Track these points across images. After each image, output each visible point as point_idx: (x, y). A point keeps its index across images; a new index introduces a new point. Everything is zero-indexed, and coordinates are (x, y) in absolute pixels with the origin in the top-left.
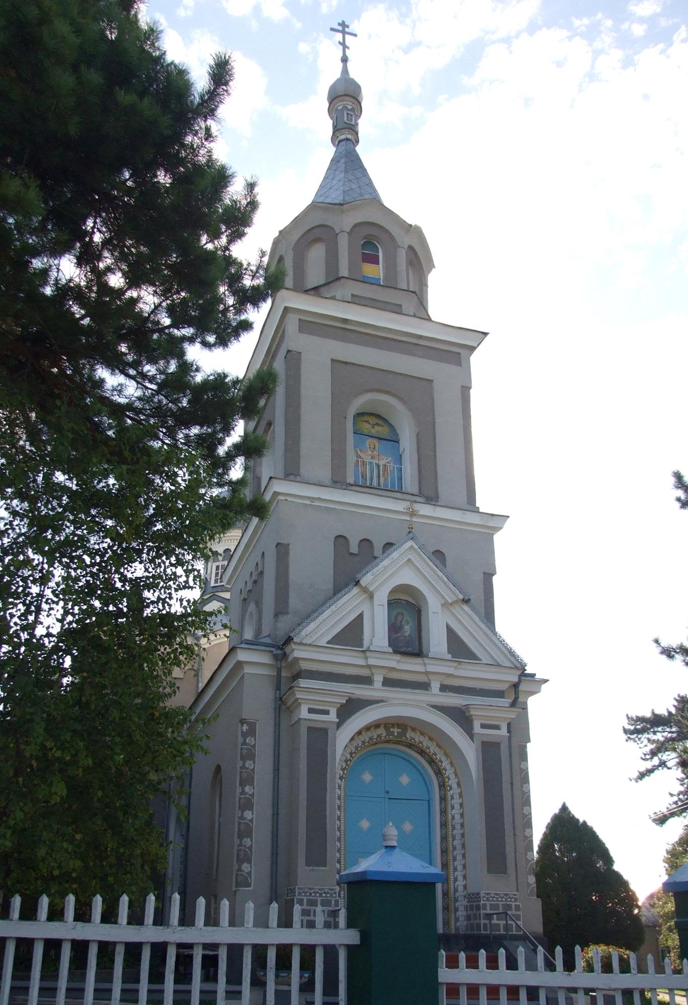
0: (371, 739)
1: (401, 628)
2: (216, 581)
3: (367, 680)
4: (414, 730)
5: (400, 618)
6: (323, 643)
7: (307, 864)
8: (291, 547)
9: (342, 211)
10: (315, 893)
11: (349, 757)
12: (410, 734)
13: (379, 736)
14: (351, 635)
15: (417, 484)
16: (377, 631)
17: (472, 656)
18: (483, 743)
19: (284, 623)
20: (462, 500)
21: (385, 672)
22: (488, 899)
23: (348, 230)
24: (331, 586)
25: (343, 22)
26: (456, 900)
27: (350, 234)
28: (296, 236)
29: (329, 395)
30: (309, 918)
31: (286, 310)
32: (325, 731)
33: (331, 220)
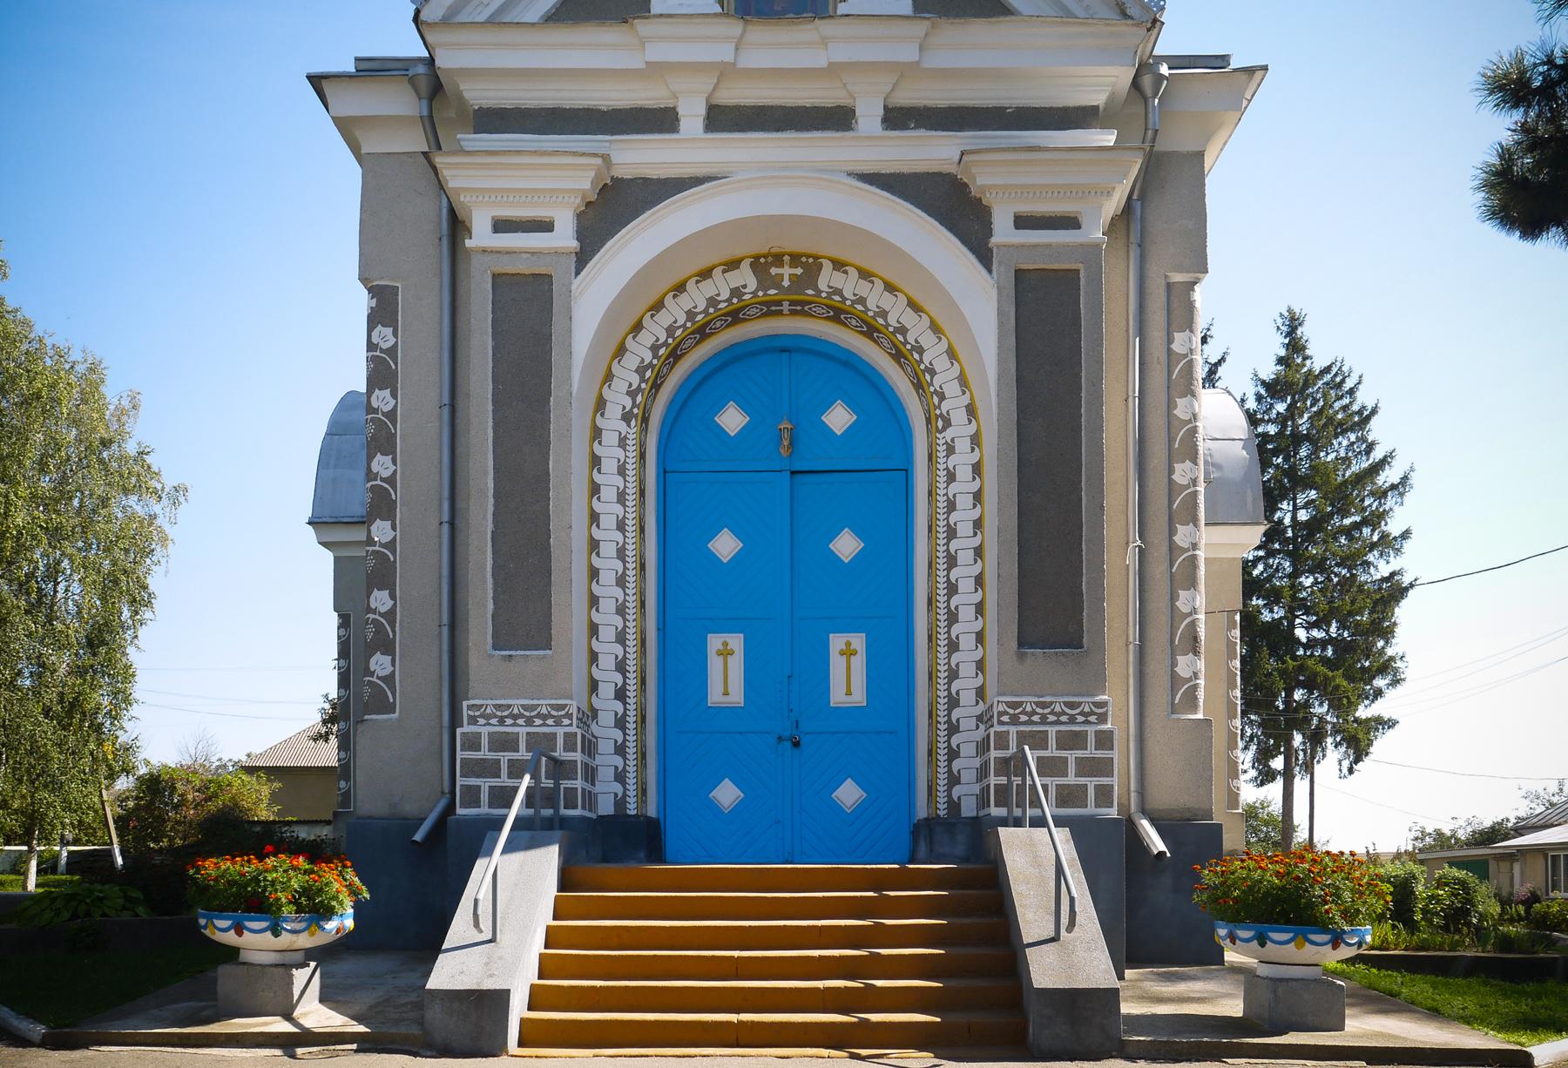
3: (661, 120)
4: (839, 265)
10: (515, 717)
12: (827, 279)
18: (1020, 274)
22: (1014, 721)
26: (953, 729)
30: (494, 782)
32: (544, 280)
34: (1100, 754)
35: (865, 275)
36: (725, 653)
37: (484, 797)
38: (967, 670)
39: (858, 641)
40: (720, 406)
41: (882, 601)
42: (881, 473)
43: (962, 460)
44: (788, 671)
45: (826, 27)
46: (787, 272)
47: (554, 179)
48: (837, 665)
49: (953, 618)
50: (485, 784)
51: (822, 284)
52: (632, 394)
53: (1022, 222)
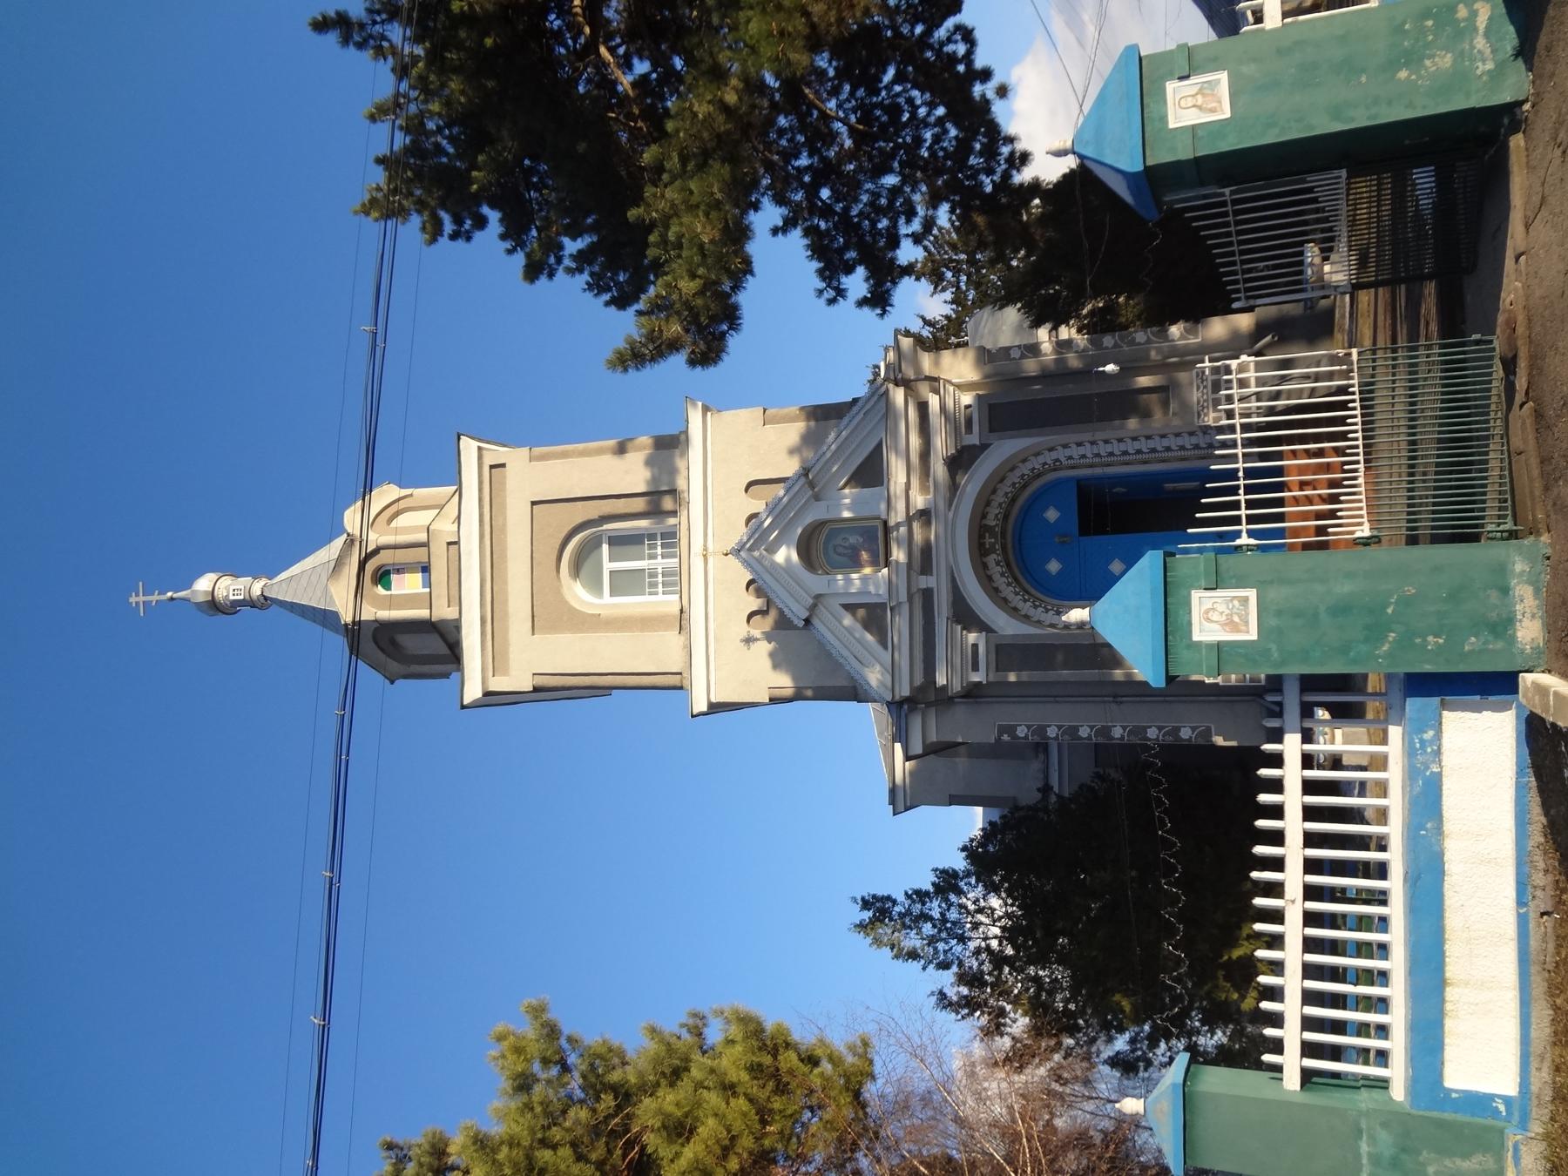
3: (927, 594)
4: (984, 516)
5: (840, 550)
12: (991, 521)
18: (991, 430)
21: (914, 575)
35: (1148, 437)
38: (1180, 441)
40: (1048, 573)
43: (1075, 452)
49: (1153, 450)
52: (1047, 611)
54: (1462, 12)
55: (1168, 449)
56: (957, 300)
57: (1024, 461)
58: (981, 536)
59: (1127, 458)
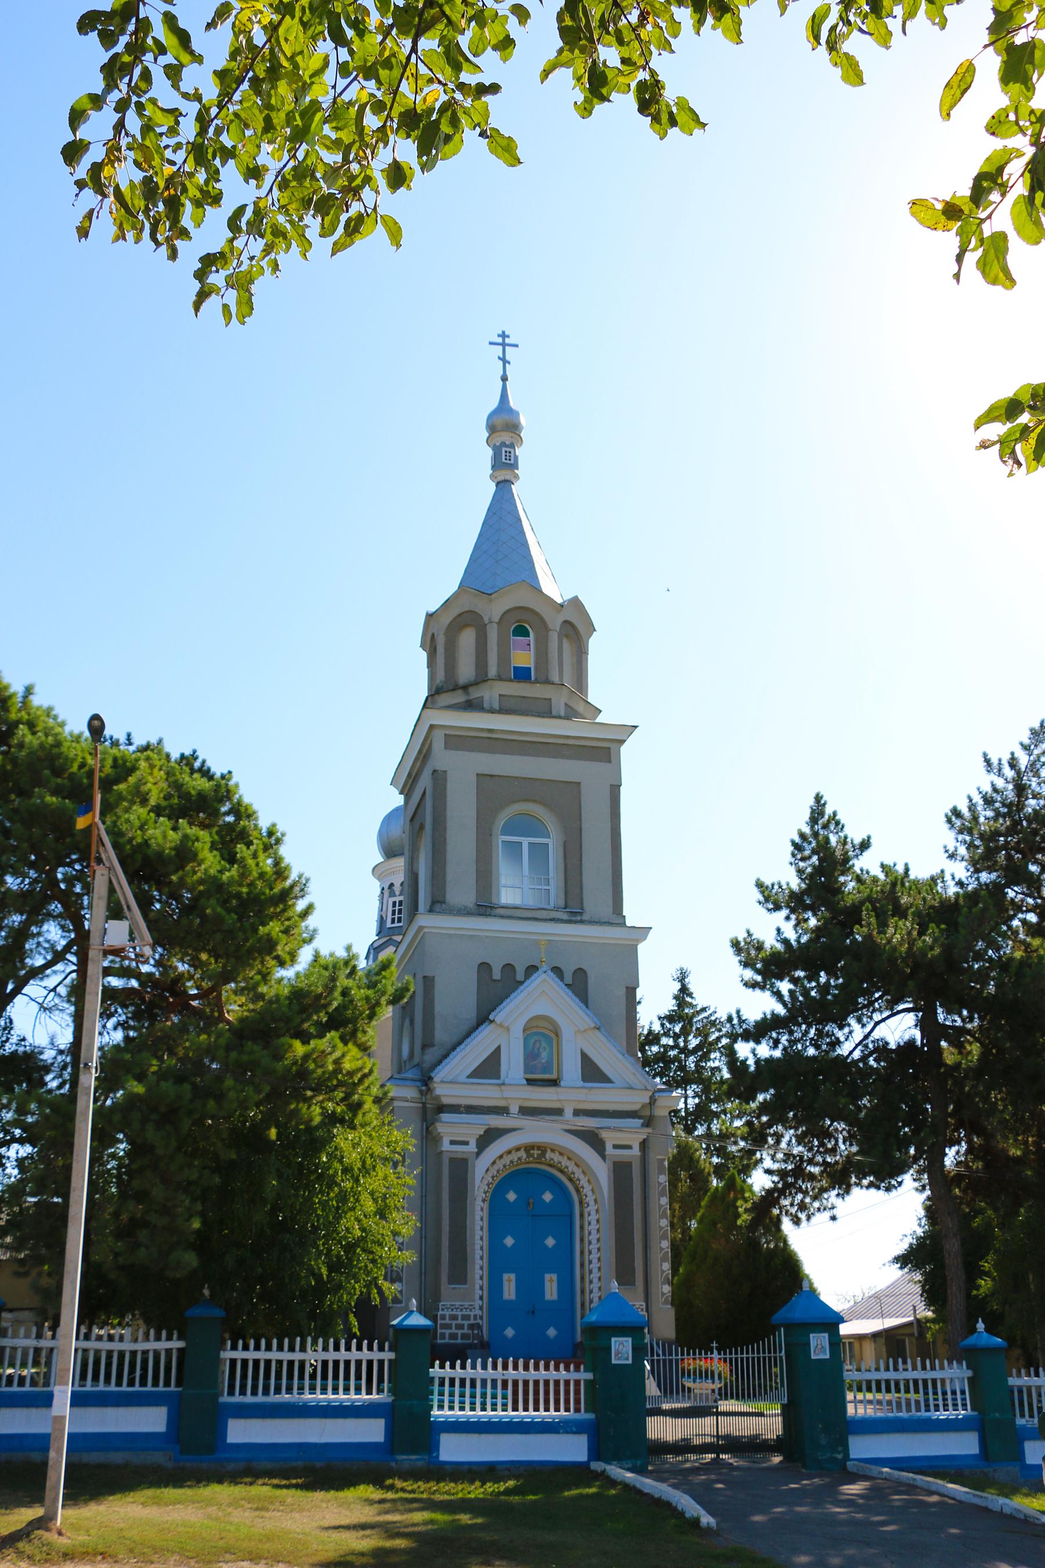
0: (512, 1162)
1: (538, 1055)
2: (393, 922)
4: (553, 1151)
5: (538, 1044)
6: (463, 1078)
7: (450, 1283)
8: (436, 979)
9: (491, 601)
11: (491, 1180)
12: (549, 1155)
13: (519, 1159)
14: (489, 1068)
15: (562, 896)
16: (513, 1066)
17: (604, 1079)
18: (615, 1163)
19: (430, 1056)
20: (607, 911)
23: (497, 620)
24: (474, 1014)
25: (504, 332)
27: (498, 623)
28: (446, 620)
29: (473, 814)
31: (432, 727)
33: (480, 606)
34: (45, 1389)
36: (509, 1280)
37: (447, 1336)
39: (554, 1277)
41: (565, 1263)
42: (564, 1215)
44: (530, 1287)
45: (558, 1089)
46: (536, 1152)
47: (471, 1128)
48: (547, 1285)
50: (447, 1332)
51: (547, 1156)
53: (615, 1147)
54: (840, 1449)
55: (591, 1282)
56: (652, 1038)
57: (569, 1159)
58: (539, 1148)
59: (586, 1253)
